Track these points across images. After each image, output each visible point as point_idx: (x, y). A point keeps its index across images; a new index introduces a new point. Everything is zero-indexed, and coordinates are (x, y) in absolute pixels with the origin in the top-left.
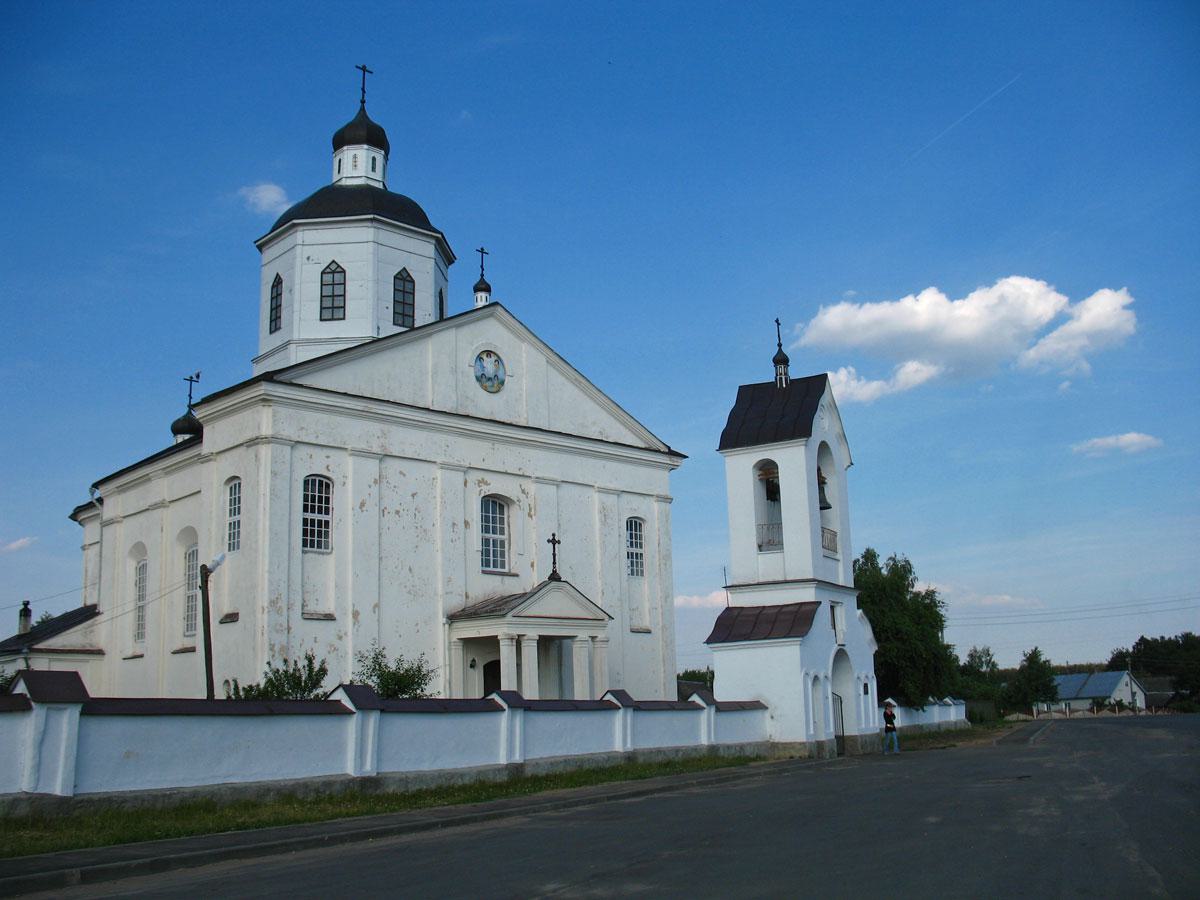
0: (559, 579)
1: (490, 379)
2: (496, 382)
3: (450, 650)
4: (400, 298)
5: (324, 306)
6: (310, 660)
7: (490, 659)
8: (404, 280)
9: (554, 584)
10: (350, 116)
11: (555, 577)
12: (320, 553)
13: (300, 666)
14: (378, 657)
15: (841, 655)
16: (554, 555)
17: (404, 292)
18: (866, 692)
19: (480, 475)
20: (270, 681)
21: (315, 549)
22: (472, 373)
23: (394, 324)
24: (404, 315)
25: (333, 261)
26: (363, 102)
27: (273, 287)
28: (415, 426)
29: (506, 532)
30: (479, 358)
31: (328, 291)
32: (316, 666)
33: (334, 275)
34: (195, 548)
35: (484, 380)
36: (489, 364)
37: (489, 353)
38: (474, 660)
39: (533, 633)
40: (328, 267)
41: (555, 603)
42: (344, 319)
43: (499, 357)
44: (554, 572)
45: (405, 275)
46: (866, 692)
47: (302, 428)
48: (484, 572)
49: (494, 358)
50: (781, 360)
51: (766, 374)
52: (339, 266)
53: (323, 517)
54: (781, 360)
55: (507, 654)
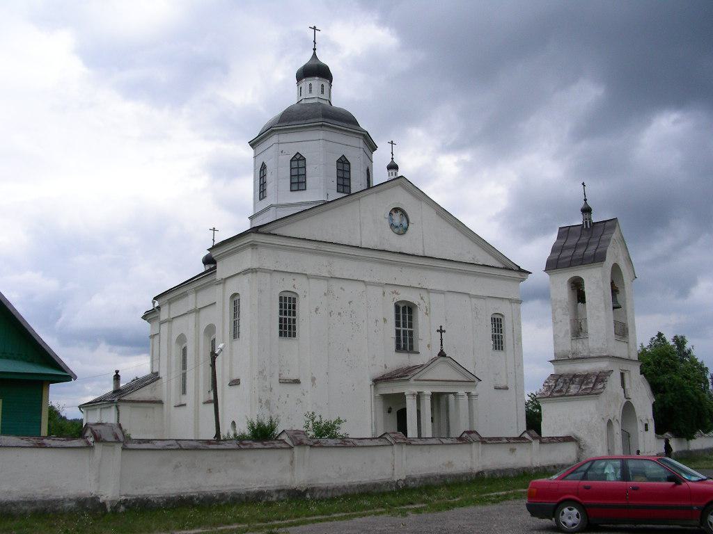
1: (397, 227)
2: (401, 229)
7: (401, 407)
8: (343, 163)
9: (442, 359)
10: (305, 59)
11: (442, 354)
15: (628, 408)
18: (646, 429)
19: (393, 289)
25: (298, 153)
26: (315, 49)
31: (295, 172)
33: (298, 162)
36: (397, 219)
37: (396, 210)
39: (428, 391)
41: (442, 371)
42: (305, 189)
44: (442, 351)
45: (343, 159)
46: (646, 429)
49: (399, 213)
50: (587, 210)
54: (587, 210)
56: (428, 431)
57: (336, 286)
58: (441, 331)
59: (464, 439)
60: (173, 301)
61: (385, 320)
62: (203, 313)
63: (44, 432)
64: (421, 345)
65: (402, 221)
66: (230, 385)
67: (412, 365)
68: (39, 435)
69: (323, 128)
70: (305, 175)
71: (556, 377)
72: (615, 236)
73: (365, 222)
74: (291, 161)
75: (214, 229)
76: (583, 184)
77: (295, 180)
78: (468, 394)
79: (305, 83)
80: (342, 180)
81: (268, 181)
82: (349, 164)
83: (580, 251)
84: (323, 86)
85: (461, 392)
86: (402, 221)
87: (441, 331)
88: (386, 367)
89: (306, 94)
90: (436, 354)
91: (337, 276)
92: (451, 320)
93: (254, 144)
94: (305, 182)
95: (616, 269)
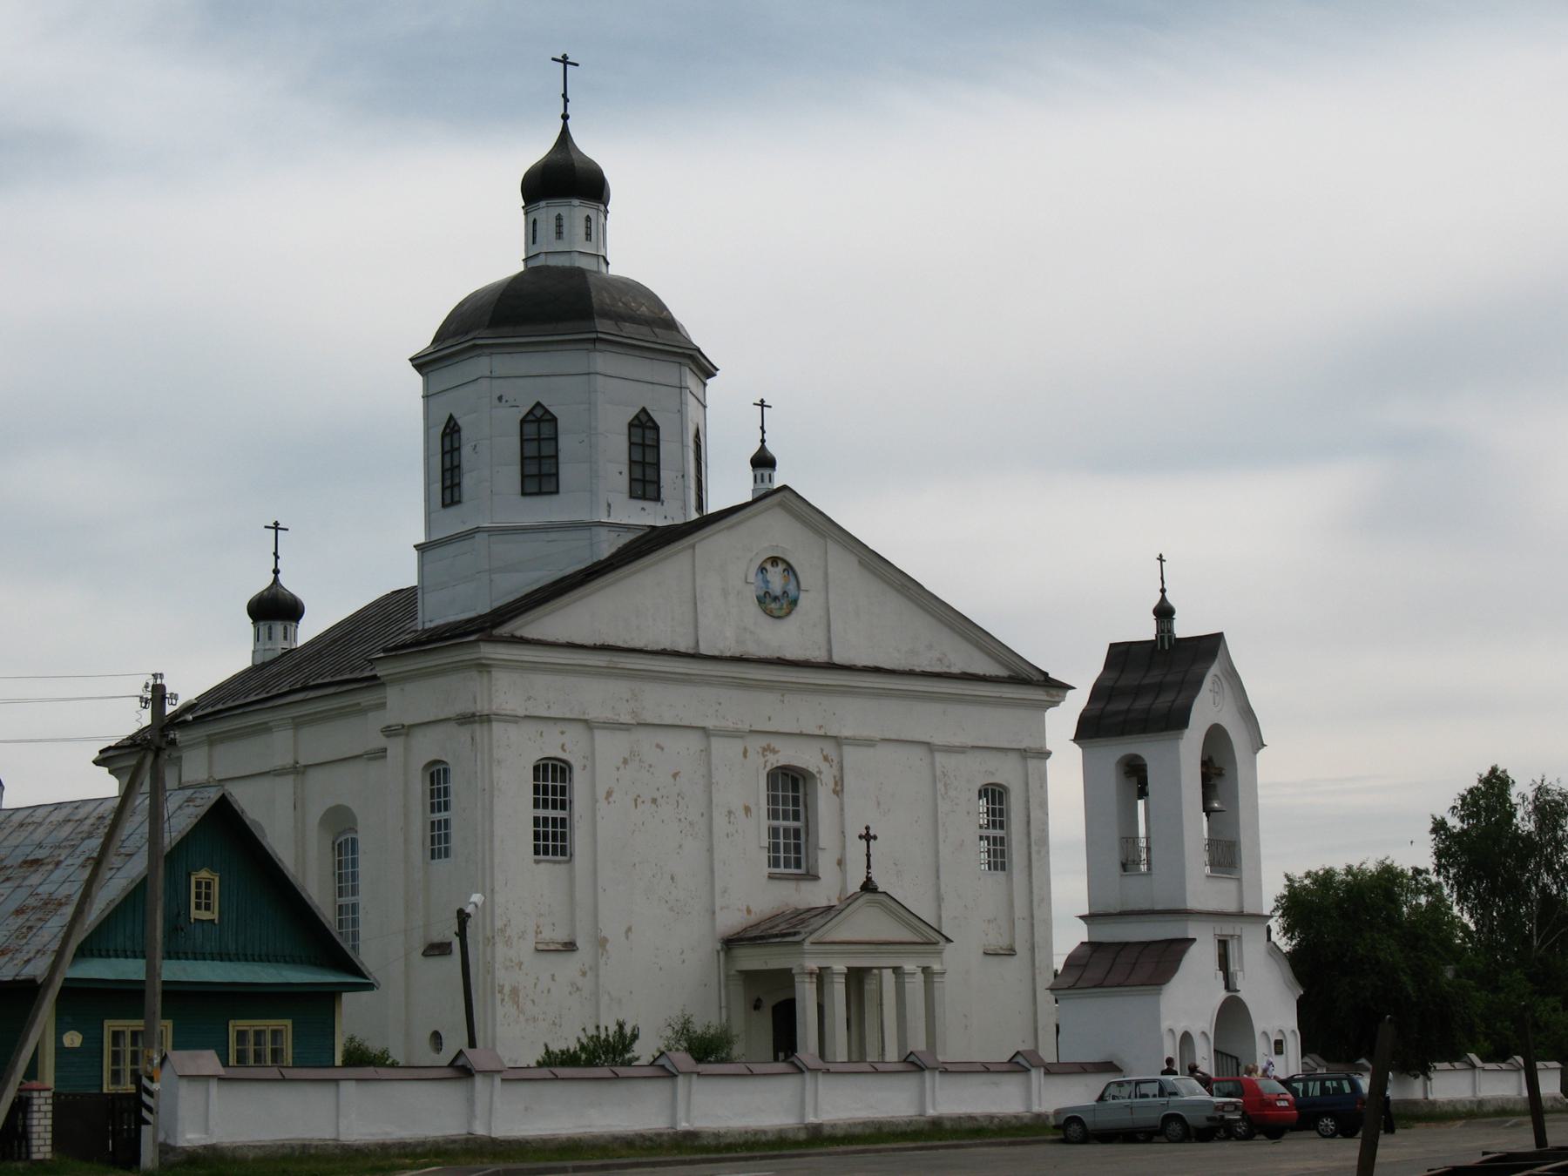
0: (875, 890)
1: (776, 599)
2: (785, 602)
3: (727, 986)
4: (650, 474)
5: (527, 454)
6: (621, 1026)
7: (782, 997)
9: (868, 896)
11: (868, 887)
12: (555, 862)
13: (611, 1033)
14: (687, 1022)
16: (868, 856)
17: (643, 445)
19: (763, 741)
20: (583, 1047)
21: (550, 857)
22: (751, 593)
23: (631, 497)
24: (644, 481)
25: (538, 404)
26: (565, 117)
27: (444, 435)
28: (676, 681)
29: (802, 817)
30: (762, 569)
31: (531, 450)
32: (628, 1030)
33: (539, 430)
34: (349, 836)
35: (768, 600)
36: (776, 577)
37: (775, 560)
38: (759, 1000)
39: (840, 966)
40: (531, 412)
41: (866, 924)
42: (557, 492)
43: (789, 565)
44: (869, 879)
45: (644, 418)
47: (529, 698)
48: (771, 877)
49: (781, 567)
50: (1164, 613)
51: (1146, 630)
52: (547, 411)
53: (541, 813)
54: (1164, 613)
55: (806, 995)
56: (842, 1055)
57: (646, 740)
58: (868, 837)
59: (914, 1065)
60: (222, 741)
61: (747, 810)
62: (315, 777)
63: (338, 1061)
64: (825, 864)
65: (787, 583)
66: (425, 954)
67: (803, 906)
68: (333, 1066)
69: (598, 346)
70: (556, 457)
71: (1092, 948)
72: (1215, 669)
73: (700, 596)
74: (523, 421)
75: (276, 527)
76: (1161, 559)
77: (532, 469)
78: (925, 970)
79: (547, 212)
80: (640, 450)
81: (465, 465)
82: (656, 428)
83: (1142, 704)
84: (588, 219)
85: (909, 966)
86: (787, 583)
87: (868, 837)
88: (749, 911)
89: (547, 242)
90: (855, 885)
91: (649, 721)
92: (892, 809)
93: (422, 363)
94: (557, 475)
95: (1216, 737)
